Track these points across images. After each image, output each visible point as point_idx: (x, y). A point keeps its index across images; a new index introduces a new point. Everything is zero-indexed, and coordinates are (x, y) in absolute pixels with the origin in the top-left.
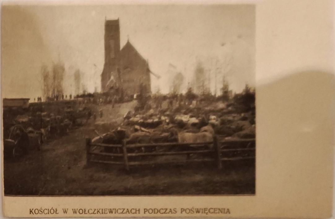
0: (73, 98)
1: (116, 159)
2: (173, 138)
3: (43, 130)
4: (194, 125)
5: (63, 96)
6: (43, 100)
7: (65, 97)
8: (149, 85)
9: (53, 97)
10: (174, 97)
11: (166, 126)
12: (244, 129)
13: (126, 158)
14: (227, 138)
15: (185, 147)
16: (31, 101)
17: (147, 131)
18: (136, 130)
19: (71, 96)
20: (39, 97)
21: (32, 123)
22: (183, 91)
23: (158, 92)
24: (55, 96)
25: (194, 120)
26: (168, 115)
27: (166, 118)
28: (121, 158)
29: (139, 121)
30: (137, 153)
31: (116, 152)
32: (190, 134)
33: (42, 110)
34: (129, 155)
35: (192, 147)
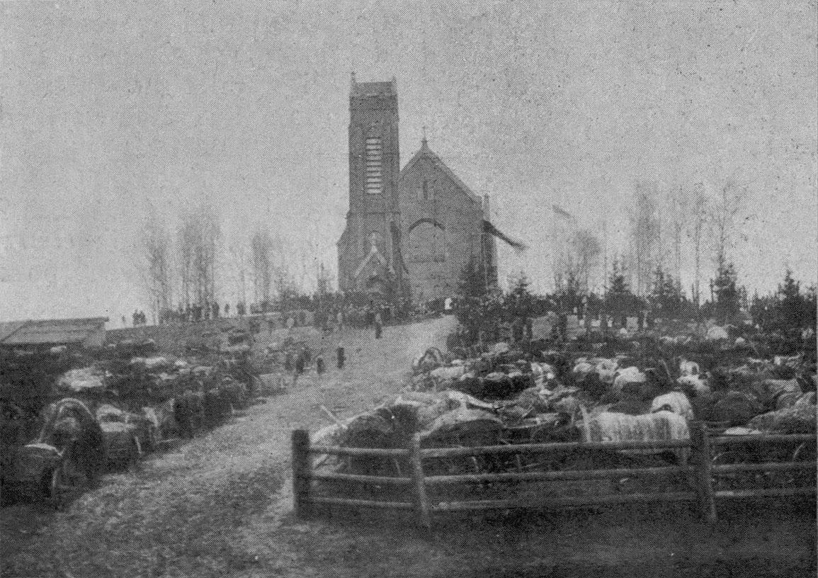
0: (248, 314)
1: (390, 490)
2: (565, 428)
3: (151, 414)
4: (630, 388)
5: (216, 308)
6: (152, 320)
7: (222, 311)
8: (492, 270)
9: (184, 308)
10: (570, 300)
11: (544, 391)
12: (782, 406)
13: (421, 490)
14: (730, 431)
15: (608, 456)
16: (115, 325)
17: (490, 406)
18: (452, 405)
19: (241, 308)
20: (139, 313)
21: (115, 392)
22: (598, 286)
23: (520, 290)
24: (191, 307)
25: (631, 375)
26: (551, 360)
27: (547, 366)
28: (406, 489)
29: (463, 378)
30: (454, 474)
31: (392, 471)
32: (621, 417)
33: (145, 350)
34: (427, 479)
35: (627, 458)
